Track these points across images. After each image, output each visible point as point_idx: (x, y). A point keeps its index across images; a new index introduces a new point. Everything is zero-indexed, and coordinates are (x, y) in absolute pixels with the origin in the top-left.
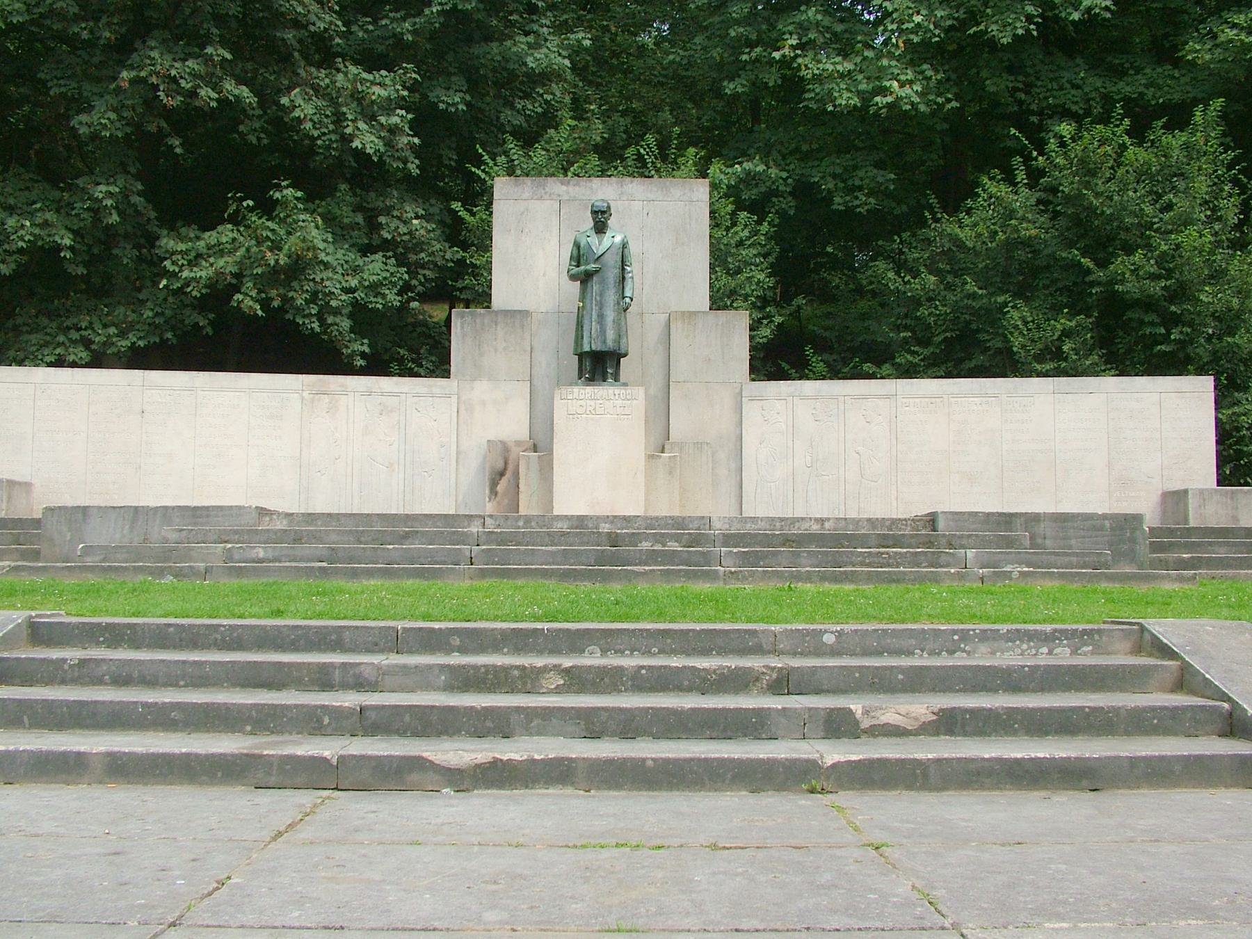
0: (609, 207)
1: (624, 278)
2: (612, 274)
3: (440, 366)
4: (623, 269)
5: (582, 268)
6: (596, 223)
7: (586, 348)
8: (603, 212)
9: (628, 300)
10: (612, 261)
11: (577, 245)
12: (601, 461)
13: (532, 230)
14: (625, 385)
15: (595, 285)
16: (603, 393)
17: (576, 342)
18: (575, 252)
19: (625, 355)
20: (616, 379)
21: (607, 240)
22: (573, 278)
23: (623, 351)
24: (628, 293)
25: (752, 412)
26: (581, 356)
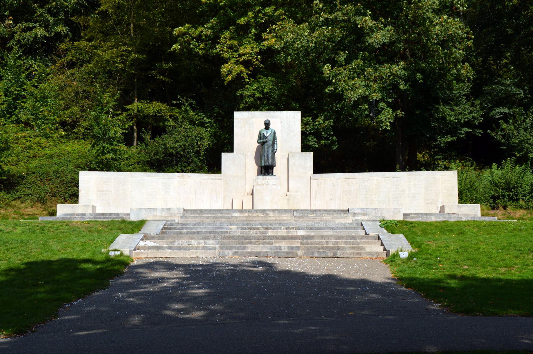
2: (270, 143)
10: (271, 138)
11: (260, 133)
12: (271, 194)
13: (247, 125)
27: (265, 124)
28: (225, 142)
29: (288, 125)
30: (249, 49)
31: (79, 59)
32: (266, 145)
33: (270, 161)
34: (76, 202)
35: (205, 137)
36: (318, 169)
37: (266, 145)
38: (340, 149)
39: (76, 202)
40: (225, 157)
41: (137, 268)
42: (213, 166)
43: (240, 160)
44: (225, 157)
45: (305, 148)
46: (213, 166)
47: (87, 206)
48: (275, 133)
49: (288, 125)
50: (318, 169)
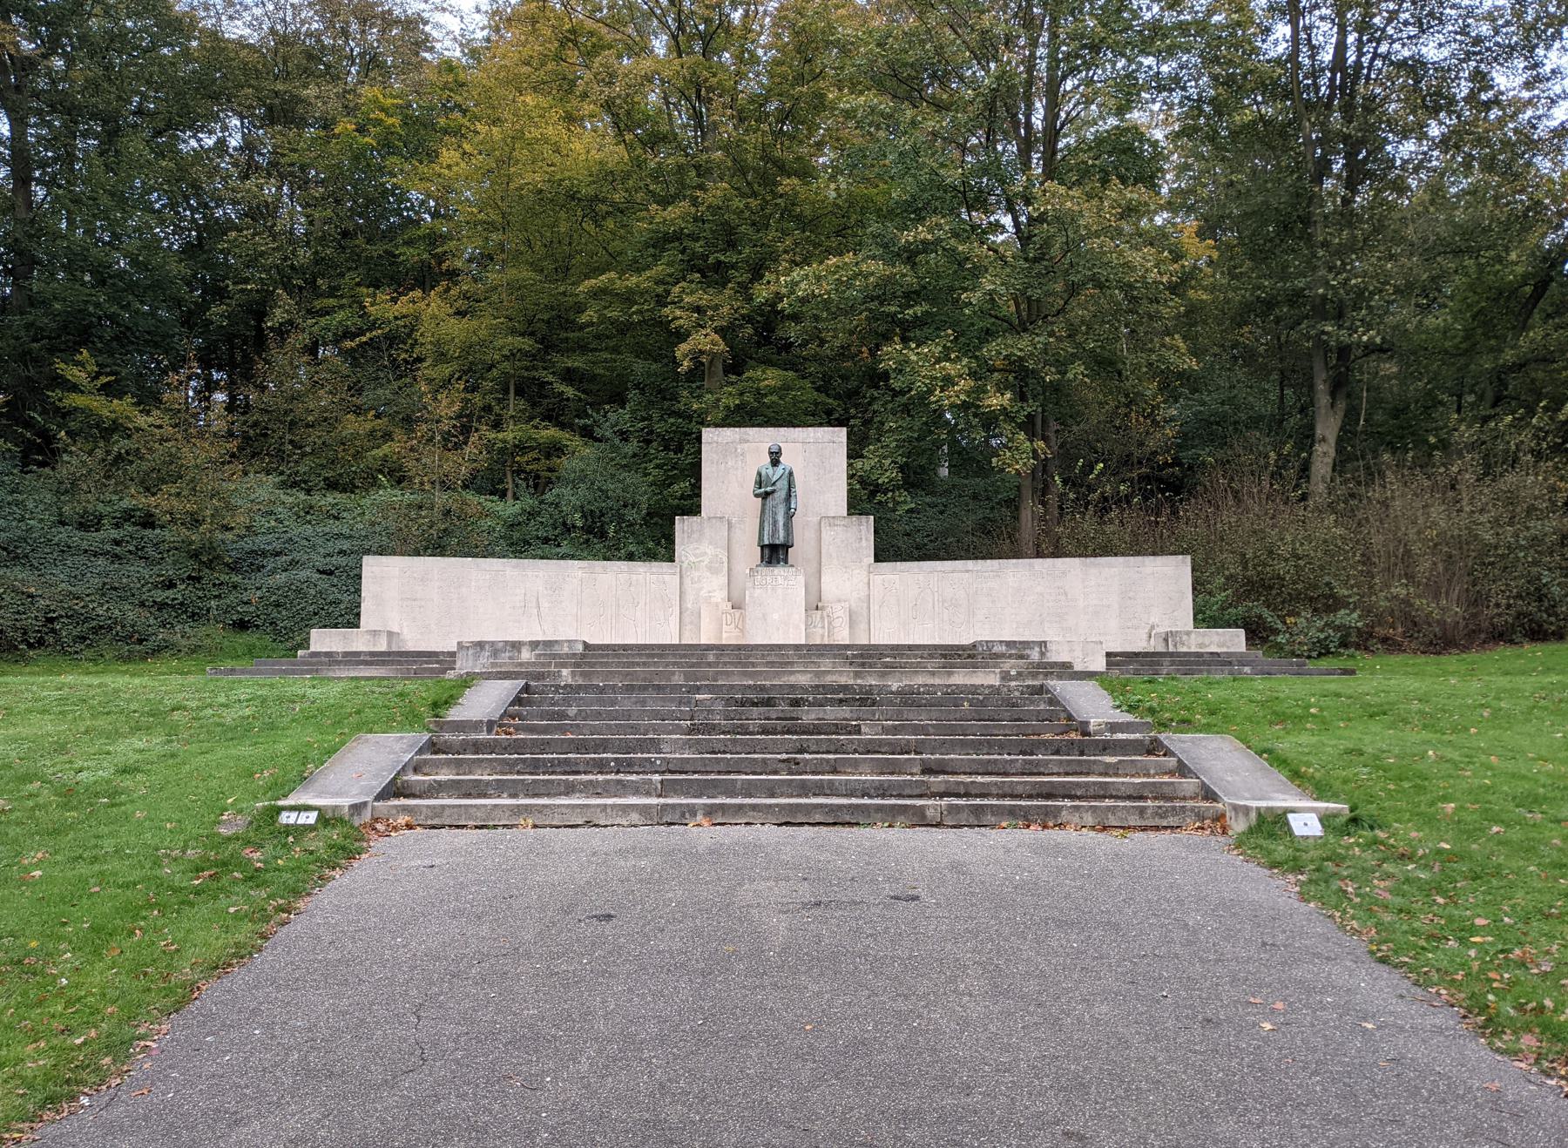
2: (781, 494)
10: (783, 484)
11: (759, 474)
12: (777, 614)
13: (732, 459)
16: (779, 571)
21: (780, 470)
22: (757, 496)
26: (763, 547)
27: (771, 453)
28: (682, 494)
29: (818, 458)
30: (726, 304)
31: (880, 1052)
32: (774, 492)
33: (782, 533)
34: (354, 623)
35: (640, 488)
36: (883, 553)
37: (774, 492)
38: (923, 509)
39: (354, 623)
40: (682, 525)
41: (1129, 724)
42: (660, 546)
43: (715, 539)
44: (682, 525)
45: (855, 506)
46: (660, 546)
47: (375, 633)
48: (791, 474)
49: (818, 458)
50: (883, 553)
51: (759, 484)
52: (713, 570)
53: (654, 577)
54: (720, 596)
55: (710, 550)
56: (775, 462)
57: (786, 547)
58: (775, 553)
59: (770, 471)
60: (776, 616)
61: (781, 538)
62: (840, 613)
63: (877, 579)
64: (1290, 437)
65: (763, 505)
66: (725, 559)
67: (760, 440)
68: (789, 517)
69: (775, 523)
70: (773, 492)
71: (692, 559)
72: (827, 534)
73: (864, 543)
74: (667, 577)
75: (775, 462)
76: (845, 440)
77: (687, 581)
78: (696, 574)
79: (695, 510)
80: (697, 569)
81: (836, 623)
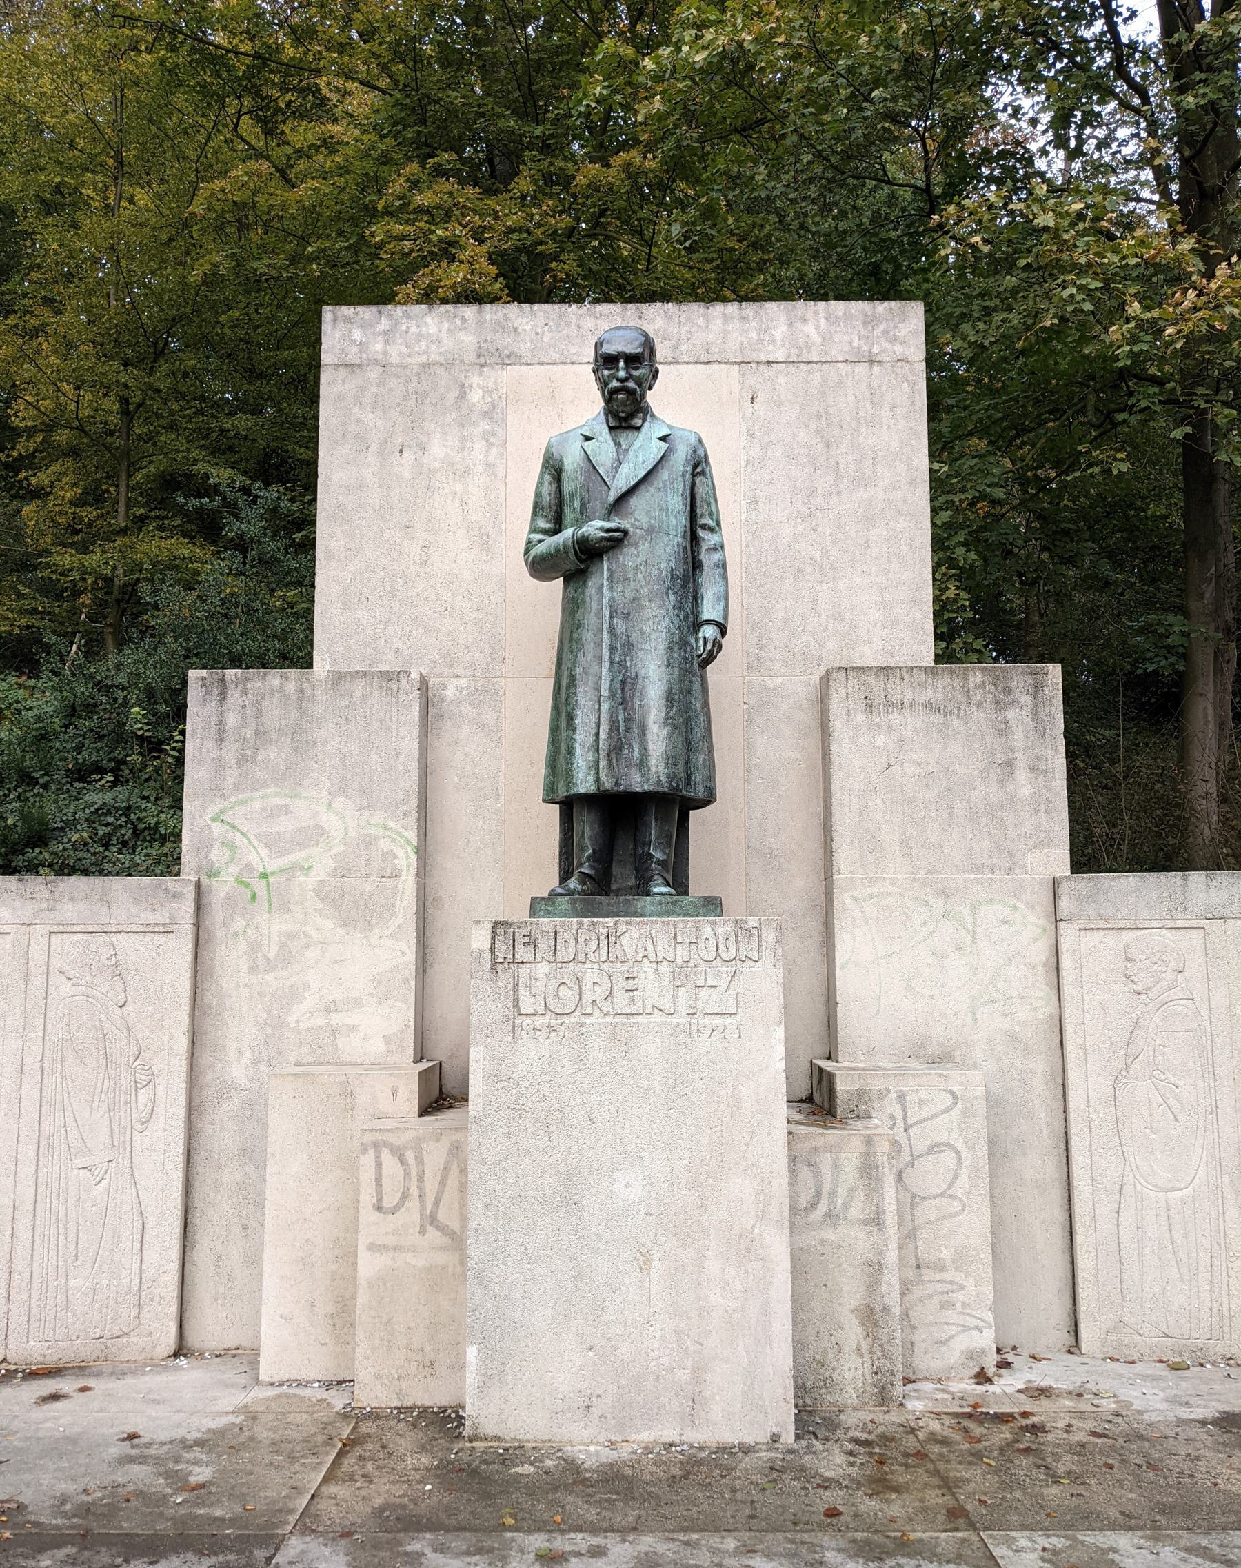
0: (649, 345)
1: (697, 565)
2: (651, 555)
3: (143, 839)
4: (694, 539)
5: (568, 533)
6: (610, 397)
7: (584, 783)
8: (633, 360)
9: (709, 632)
10: (660, 510)
11: (554, 469)
12: (637, 1252)
13: (442, 435)
14: (712, 906)
15: (601, 588)
16: (645, 939)
17: (552, 764)
18: (547, 490)
19: (707, 800)
20: (680, 884)
21: (644, 447)
22: (541, 567)
23: (700, 792)
24: (709, 611)
25: (1089, 951)
26: (569, 806)
27: (606, 361)
33: (657, 741)
40: (223, 717)
43: (353, 782)
45: (981, 617)
48: (698, 465)
51: (553, 510)
52: (350, 908)
53: (69, 945)
54: (379, 1031)
55: (339, 820)
56: (625, 409)
57: (678, 804)
58: (626, 839)
59: (603, 448)
60: (629, 1187)
61: (653, 764)
62: (944, 1128)
63: (1089, 951)
64: (1074, 1539)
65: (572, 608)
66: (406, 860)
67: (544, 363)
68: (694, 658)
69: (625, 688)
70: (616, 541)
71: (259, 858)
72: (857, 746)
73: (1023, 784)
74: (130, 947)
75: (625, 409)
76: (916, 350)
77: (230, 961)
78: (272, 927)
79: (284, 641)
80: (278, 903)
81: (931, 1175)
